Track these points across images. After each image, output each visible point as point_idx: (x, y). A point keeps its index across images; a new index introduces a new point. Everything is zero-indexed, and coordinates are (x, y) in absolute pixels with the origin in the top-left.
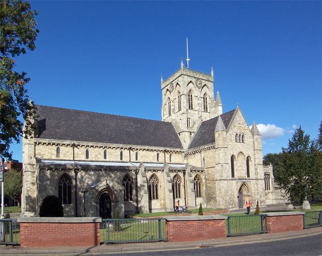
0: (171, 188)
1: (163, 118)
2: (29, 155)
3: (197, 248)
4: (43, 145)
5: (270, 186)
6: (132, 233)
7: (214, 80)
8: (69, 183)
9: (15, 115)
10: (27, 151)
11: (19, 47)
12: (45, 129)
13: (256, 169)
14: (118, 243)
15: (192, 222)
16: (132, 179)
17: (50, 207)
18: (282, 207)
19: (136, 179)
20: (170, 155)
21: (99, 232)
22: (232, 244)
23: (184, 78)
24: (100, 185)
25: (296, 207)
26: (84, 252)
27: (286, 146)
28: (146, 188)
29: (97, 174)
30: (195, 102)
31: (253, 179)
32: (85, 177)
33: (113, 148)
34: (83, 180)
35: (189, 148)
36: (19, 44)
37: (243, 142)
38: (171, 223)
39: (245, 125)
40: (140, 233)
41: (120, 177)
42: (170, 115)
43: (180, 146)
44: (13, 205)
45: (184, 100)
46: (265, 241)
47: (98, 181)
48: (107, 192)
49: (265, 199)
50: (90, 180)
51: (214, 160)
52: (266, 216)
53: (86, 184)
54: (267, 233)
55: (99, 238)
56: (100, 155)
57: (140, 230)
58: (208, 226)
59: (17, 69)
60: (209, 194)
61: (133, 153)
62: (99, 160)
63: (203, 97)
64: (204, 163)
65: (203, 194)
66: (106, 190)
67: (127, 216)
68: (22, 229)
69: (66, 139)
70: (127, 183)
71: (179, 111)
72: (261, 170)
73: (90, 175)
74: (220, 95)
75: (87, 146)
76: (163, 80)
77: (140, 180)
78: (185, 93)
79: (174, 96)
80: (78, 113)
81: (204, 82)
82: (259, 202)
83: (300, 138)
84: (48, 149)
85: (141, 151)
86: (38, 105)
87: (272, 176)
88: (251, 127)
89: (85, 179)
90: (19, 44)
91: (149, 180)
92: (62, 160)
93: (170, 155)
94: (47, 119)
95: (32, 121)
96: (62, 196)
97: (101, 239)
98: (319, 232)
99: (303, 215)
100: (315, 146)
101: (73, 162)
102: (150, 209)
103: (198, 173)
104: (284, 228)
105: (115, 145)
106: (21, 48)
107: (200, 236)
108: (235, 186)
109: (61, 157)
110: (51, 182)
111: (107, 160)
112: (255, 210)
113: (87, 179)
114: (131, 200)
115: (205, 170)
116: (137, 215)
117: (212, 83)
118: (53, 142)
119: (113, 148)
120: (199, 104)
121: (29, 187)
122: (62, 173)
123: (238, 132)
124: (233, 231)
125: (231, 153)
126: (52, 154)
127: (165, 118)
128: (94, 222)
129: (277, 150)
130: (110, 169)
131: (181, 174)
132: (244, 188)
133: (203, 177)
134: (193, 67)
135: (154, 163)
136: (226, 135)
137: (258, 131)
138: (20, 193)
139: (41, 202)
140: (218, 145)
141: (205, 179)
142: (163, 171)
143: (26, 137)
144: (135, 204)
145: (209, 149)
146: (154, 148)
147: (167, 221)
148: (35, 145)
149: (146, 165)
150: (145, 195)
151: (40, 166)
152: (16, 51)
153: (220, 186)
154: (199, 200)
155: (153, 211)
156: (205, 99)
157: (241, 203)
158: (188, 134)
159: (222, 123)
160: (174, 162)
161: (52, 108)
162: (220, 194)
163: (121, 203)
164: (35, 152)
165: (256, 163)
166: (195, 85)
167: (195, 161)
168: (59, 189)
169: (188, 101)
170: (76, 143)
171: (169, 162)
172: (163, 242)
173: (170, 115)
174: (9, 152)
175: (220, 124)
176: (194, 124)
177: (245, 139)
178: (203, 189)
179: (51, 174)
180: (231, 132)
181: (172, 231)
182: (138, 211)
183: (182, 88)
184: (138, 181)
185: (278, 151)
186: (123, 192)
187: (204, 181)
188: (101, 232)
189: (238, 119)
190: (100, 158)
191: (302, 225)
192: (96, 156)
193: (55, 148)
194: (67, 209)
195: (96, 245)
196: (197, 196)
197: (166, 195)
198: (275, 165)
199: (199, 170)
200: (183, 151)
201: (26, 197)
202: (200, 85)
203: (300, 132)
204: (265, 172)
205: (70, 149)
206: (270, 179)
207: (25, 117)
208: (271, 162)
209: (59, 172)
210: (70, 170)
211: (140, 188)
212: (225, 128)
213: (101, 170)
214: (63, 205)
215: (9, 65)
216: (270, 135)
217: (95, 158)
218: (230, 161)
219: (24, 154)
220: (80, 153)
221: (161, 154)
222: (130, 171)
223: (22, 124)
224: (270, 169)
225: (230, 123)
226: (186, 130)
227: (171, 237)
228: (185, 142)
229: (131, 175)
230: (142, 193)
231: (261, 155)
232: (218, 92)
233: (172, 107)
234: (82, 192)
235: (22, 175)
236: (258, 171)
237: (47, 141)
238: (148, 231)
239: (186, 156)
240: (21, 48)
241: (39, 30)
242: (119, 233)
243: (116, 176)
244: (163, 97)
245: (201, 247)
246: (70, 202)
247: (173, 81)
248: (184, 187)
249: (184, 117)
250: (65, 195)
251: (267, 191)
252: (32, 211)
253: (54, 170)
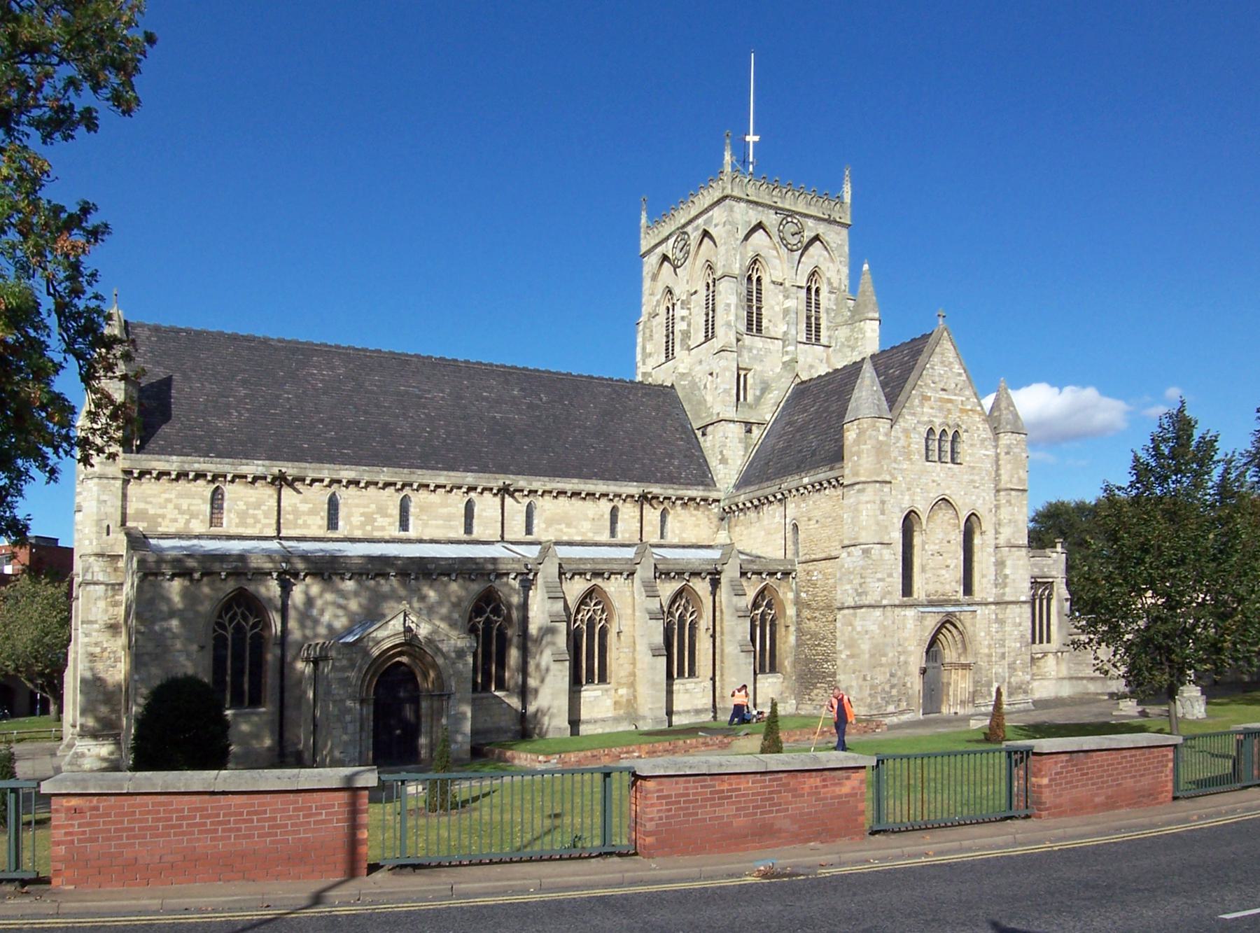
0: (659, 639)
1: (641, 369)
2: (99, 521)
3: (750, 880)
4: (158, 478)
5: (1054, 628)
6: (497, 817)
7: (853, 217)
8: (254, 626)
9: (44, 373)
10: (94, 503)
11: (72, 106)
12: (166, 416)
13: (1000, 564)
14: (439, 866)
15: (734, 779)
16: (509, 606)
17: (175, 726)
18: (1095, 709)
19: (524, 606)
20: (664, 515)
21: (366, 826)
22: (887, 865)
23: (731, 209)
24: (380, 634)
25: (1149, 709)
26: (304, 903)
27: (1123, 478)
28: (561, 640)
29: (367, 588)
30: (773, 304)
31: (986, 604)
32: (319, 603)
33: (437, 487)
34: (315, 612)
35: (737, 487)
36: (71, 92)
37: (953, 461)
38: (650, 785)
39: (968, 393)
40: (527, 816)
41: (460, 600)
42: (669, 354)
43: (703, 476)
44: (32, 713)
45: (729, 296)
46: (1020, 850)
47: (373, 615)
48: (404, 659)
49: (1028, 677)
50: (340, 612)
51: (835, 533)
52: (1028, 753)
53: (322, 630)
54: (1027, 817)
55: (363, 849)
56: (385, 515)
57: (528, 806)
58: (796, 794)
59: (61, 193)
60: (808, 661)
61: (516, 508)
62: (377, 534)
63: (804, 284)
64: (796, 543)
65: (786, 660)
66: (400, 654)
67: (484, 751)
68: (58, 819)
69: (248, 456)
70: (488, 622)
71: (707, 339)
72: (1020, 570)
73: (342, 594)
74: (876, 282)
75: (333, 481)
76: (649, 218)
77: (540, 610)
78: (736, 269)
79: (688, 280)
80: (302, 353)
81: (811, 228)
82: (1004, 691)
83: (1179, 446)
84: (179, 496)
85: (547, 497)
86: (142, 326)
87: (1060, 590)
88: (988, 402)
89: (322, 612)
90: (71, 92)
91: (573, 611)
92: (230, 537)
93: (664, 515)
94: (177, 377)
95: (118, 391)
96: (228, 679)
97: (370, 853)
98: (1233, 811)
99: (1175, 746)
100: (1237, 479)
101: (274, 545)
102: (575, 722)
103: (770, 581)
104: (1097, 800)
105: (443, 478)
106: (78, 108)
107: (764, 834)
108: (913, 629)
109: (230, 523)
110: (184, 622)
111: (412, 533)
112: (988, 722)
113: (329, 610)
114: (497, 688)
115: (798, 567)
116: (523, 746)
117: (845, 232)
118: (196, 466)
119: (437, 487)
120: (786, 312)
121: (97, 644)
122: (231, 585)
123: (937, 421)
124: (896, 811)
125: (906, 505)
126: (193, 515)
127: (650, 366)
128: (349, 788)
129: (1083, 489)
130: (420, 572)
131: (701, 587)
132: (947, 638)
133: (787, 595)
134: (774, 168)
135: (596, 544)
136: (886, 435)
137: (1016, 416)
138: (59, 667)
139: (141, 701)
140: (856, 474)
141: (797, 602)
142: (632, 574)
143: (86, 460)
144: (515, 702)
145: (819, 487)
146: (599, 487)
147: (636, 777)
148: (126, 482)
149: (563, 552)
150: (555, 667)
151: (142, 562)
152: (60, 123)
153: (854, 629)
154: (769, 687)
155: (584, 729)
156: (811, 292)
157: (933, 694)
158: (736, 430)
159: (877, 387)
160: (676, 541)
161: (199, 334)
162: (851, 662)
163: (461, 701)
164: (124, 508)
165: (1002, 541)
166: (776, 239)
167: (762, 535)
168: (216, 648)
169: (744, 303)
170: (290, 469)
171: (655, 539)
172: (616, 859)
173: (669, 354)
174: (20, 514)
175: (867, 390)
176: (763, 391)
177: (962, 448)
178: (788, 641)
179: (185, 594)
180: (907, 421)
181: (653, 811)
182: (525, 729)
183: (722, 249)
184: (531, 614)
185: (1091, 494)
186: (470, 660)
187: (791, 611)
188: (374, 814)
189: (939, 369)
190: (383, 528)
191: (1170, 786)
192: (369, 519)
193: (204, 489)
194: (245, 727)
195: (352, 873)
196: (763, 671)
197: (639, 665)
198: (1076, 547)
199: (772, 568)
200: (714, 495)
201: (83, 681)
202: (794, 240)
203: (1181, 424)
204: (1036, 572)
205: (265, 493)
206: (1054, 603)
207: (88, 378)
208: (1063, 534)
209: (219, 585)
210: (262, 574)
211: (538, 641)
212: (885, 405)
213: (385, 575)
214: (228, 712)
215: (30, 181)
216: (1071, 426)
217: (363, 525)
218: (897, 536)
219: (79, 516)
220: (305, 507)
221: (628, 512)
222: (500, 575)
223: (73, 410)
224: (1055, 562)
225: (908, 387)
226: (731, 413)
227: (649, 840)
228: (723, 461)
229: (503, 592)
230: (546, 658)
231: (1025, 510)
232: (866, 267)
233: (680, 326)
234: (307, 660)
235: (69, 595)
236: (1007, 571)
237: (173, 464)
238: (558, 811)
239: (726, 516)
240: (78, 108)
241: (157, 35)
242: (445, 819)
243: (444, 596)
244: (647, 284)
245: (765, 876)
246: (256, 701)
247: (690, 222)
248: (713, 636)
249: (727, 365)
250: (238, 673)
251: (1037, 647)
252: (105, 737)
253: (197, 576)
